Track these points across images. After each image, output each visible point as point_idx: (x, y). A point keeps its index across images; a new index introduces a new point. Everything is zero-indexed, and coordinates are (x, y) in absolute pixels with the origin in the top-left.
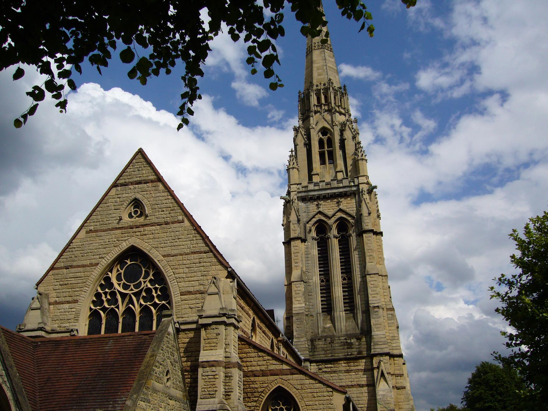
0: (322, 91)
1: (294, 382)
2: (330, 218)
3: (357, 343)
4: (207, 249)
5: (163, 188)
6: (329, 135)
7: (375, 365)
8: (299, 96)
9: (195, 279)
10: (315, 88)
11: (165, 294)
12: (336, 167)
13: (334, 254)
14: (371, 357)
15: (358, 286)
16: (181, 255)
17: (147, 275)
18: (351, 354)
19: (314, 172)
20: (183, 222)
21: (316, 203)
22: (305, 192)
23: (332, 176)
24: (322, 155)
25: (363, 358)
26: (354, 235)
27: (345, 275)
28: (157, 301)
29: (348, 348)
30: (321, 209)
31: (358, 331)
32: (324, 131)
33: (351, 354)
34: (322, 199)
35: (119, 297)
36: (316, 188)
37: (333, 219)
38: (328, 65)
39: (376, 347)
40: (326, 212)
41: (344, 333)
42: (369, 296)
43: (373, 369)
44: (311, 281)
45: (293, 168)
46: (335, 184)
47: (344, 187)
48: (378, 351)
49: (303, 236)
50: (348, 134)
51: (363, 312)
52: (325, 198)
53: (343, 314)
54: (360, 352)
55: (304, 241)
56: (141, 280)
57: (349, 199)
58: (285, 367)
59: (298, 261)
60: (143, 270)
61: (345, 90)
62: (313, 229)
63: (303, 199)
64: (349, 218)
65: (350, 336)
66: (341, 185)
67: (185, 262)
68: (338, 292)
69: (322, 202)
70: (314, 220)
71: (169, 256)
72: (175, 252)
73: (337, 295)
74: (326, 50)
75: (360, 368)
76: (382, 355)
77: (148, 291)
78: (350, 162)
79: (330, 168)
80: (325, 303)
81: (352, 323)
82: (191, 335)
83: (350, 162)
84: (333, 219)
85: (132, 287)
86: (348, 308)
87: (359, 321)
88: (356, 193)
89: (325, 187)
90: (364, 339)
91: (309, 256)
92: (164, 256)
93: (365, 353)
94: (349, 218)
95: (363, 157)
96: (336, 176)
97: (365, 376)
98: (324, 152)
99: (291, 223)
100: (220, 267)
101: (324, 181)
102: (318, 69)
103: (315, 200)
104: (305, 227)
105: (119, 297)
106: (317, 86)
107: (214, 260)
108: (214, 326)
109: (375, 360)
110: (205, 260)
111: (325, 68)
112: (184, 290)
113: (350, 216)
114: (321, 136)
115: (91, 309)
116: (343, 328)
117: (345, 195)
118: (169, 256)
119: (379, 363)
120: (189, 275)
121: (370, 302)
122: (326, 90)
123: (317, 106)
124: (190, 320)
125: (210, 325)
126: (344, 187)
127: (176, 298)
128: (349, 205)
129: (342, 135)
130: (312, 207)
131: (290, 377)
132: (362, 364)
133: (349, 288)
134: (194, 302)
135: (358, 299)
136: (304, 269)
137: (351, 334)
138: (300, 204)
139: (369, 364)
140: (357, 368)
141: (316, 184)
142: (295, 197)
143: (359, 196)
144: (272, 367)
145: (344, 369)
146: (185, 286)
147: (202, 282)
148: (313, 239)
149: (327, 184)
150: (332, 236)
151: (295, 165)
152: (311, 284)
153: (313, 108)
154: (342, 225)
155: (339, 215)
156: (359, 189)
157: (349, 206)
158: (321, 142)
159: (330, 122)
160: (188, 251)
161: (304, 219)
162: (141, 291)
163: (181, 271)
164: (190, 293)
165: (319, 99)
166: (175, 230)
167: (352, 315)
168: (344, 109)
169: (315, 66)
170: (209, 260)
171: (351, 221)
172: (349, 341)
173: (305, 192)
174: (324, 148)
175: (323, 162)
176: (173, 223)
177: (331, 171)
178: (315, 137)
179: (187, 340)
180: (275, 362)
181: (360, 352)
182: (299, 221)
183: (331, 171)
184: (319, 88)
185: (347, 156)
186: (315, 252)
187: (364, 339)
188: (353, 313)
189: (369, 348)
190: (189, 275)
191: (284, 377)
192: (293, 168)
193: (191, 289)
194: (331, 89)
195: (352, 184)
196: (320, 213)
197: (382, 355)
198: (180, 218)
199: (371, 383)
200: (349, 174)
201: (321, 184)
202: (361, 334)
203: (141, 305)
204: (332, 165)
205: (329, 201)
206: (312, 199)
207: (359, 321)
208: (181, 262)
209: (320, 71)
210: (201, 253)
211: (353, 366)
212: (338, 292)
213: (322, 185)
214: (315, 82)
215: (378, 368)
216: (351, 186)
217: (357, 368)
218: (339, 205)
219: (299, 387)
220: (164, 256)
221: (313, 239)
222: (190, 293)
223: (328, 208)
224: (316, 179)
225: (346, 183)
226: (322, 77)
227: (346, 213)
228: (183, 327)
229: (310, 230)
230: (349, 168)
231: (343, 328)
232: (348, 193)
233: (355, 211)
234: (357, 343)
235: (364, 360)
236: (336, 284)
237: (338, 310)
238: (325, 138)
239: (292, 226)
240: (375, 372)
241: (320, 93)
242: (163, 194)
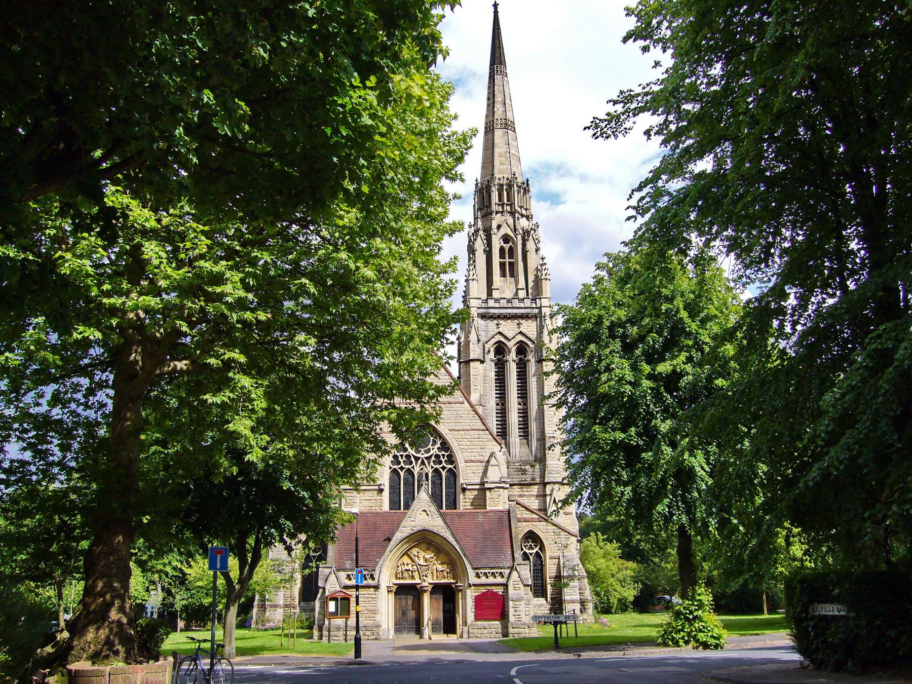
0: (505, 187)
1: (541, 527)
2: (509, 340)
3: (531, 470)
4: (484, 427)
5: (445, 372)
6: (511, 244)
7: (548, 492)
8: (477, 184)
9: (476, 450)
10: (497, 181)
11: (451, 459)
12: (517, 282)
13: (512, 379)
14: (545, 484)
15: (535, 413)
16: (463, 430)
17: (435, 443)
18: (525, 480)
19: (495, 286)
20: (463, 403)
21: (496, 322)
22: (484, 308)
23: (512, 292)
24: (502, 265)
25: (536, 484)
26: (533, 360)
27: (520, 400)
28: (444, 464)
29: (522, 474)
30: (500, 330)
31: (532, 458)
32: (506, 239)
33: (525, 480)
34: (503, 319)
35: (412, 459)
36: (497, 305)
37: (513, 342)
38: (512, 151)
39: (550, 475)
40: (505, 333)
41: (518, 458)
42: (546, 425)
43: (546, 495)
44: (487, 404)
45: (473, 280)
46: (516, 303)
47: (525, 308)
48: (552, 480)
49: (481, 357)
50: (531, 245)
51: (538, 440)
52: (506, 317)
53: (518, 440)
54: (533, 479)
55: (482, 362)
56: (430, 446)
57: (530, 321)
58: (535, 516)
59: (477, 384)
60: (431, 438)
61: (528, 185)
62: (492, 350)
63: (483, 316)
64: (529, 343)
65: (525, 463)
66: (522, 305)
67: (467, 437)
68: (514, 418)
69: (501, 322)
70: (494, 340)
71: (454, 430)
72: (459, 428)
73: (513, 421)
74: (509, 131)
75: (532, 493)
76: (554, 483)
77: (437, 456)
78: (531, 278)
79: (511, 283)
80: (499, 427)
81: (525, 449)
82: (476, 493)
83: (531, 278)
84: (513, 342)
85: (423, 452)
86: (522, 434)
87: (534, 449)
88: (538, 316)
89: (506, 306)
90: (537, 467)
91: (487, 378)
92: (450, 430)
93: (538, 480)
94: (529, 343)
95: (547, 277)
96: (516, 294)
97: (537, 501)
98: (505, 263)
99: (471, 343)
100: (495, 443)
101: (504, 298)
102: (500, 156)
103: (495, 318)
104: (484, 346)
105: (412, 459)
106: (499, 179)
107: (490, 437)
108: (496, 490)
109: (548, 488)
110: (483, 436)
111: (508, 156)
112: (468, 459)
113: (531, 340)
114: (502, 244)
115: (390, 468)
116: (518, 454)
117: (526, 317)
118: (454, 430)
119: (552, 490)
120: (471, 447)
121: (546, 432)
122: (510, 186)
123: (498, 205)
124: (473, 482)
125: (493, 488)
126: (525, 308)
127: (461, 464)
128: (530, 328)
129: (524, 245)
130: (492, 324)
131: (538, 523)
132: (535, 490)
133: (524, 414)
134: (476, 468)
135: (533, 427)
136: (482, 393)
137: (524, 461)
138: (479, 322)
139: (541, 490)
140: (529, 493)
141: (497, 300)
142: (476, 314)
143: (541, 320)
144: (524, 516)
145: (517, 493)
146: (468, 455)
147: (481, 454)
148: (492, 360)
149: (509, 301)
150: (510, 360)
151: (475, 277)
152: (488, 408)
153: (495, 208)
154: (522, 349)
155: (520, 338)
156: (541, 312)
157: (530, 329)
158: (502, 250)
159: (512, 227)
160: (469, 428)
161: (483, 339)
162: (431, 456)
163: (465, 443)
164: (472, 461)
165: (500, 199)
166: (457, 409)
167: (525, 441)
168: (526, 209)
169: (497, 150)
170: (486, 436)
171: (532, 346)
172: (523, 467)
173: (484, 308)
174: (504, 258)
175: (503, 275)
176: (455, 403)
177: (512, 286)
178: (497, 243)
179: (472, 497)
180: (527, 512)
181: (533, 479)
182: (479, 341)
183: (512, 286)
184: (501, 182)
185: (529, 270)
186: (492, 375)
187: (537, 467)
188: (528, 439)
189: (543, 476)
190: (471, 447)
191: (534, 523)
192: (473, 280)
193: (473, 459)
194: (515, 185)
195: (534, 305)
196: (500, 333)
197: (554, 483)
198: (461, 400)
199: (542, 508)
200: (530, 291)
201: (502, 301)
202: (535, 461)
203: (432, 467)
204: (513, 280)
205: (510, 321)
206: (492, 317)
207: (534, 449)
208: (464, 436)
209: (502, 158)
210: (479, 430)
211: (526, 491)
212: (514, 418)
213: (503, 303)
214: (497, 175)
215: (551, 495)
216: (532, 308)
217: (529, 493)
218: (519, 328)
219: (545, 531)
220: (450, 430)
221: (492, 360)
222: (472, 461)
223: (509, 328)
224: (496, 294)
225: (528, 303)
226: (505, 167)
227: (527, 337)
228: (469, 487)
229: (489, 351)
230: (531, 284)
231: (518, 454)
232: (530, 316)
233: (535, 336)
234: (531, 470)
235: (537, 487)
236: (512, 410)
237: (513, 436)
238: (507, 246)
239: (471, 346)
240: (548, 498)
241: (503, 189)
242: (445, 377)
